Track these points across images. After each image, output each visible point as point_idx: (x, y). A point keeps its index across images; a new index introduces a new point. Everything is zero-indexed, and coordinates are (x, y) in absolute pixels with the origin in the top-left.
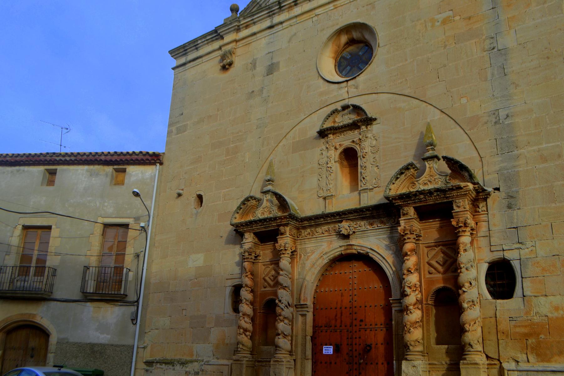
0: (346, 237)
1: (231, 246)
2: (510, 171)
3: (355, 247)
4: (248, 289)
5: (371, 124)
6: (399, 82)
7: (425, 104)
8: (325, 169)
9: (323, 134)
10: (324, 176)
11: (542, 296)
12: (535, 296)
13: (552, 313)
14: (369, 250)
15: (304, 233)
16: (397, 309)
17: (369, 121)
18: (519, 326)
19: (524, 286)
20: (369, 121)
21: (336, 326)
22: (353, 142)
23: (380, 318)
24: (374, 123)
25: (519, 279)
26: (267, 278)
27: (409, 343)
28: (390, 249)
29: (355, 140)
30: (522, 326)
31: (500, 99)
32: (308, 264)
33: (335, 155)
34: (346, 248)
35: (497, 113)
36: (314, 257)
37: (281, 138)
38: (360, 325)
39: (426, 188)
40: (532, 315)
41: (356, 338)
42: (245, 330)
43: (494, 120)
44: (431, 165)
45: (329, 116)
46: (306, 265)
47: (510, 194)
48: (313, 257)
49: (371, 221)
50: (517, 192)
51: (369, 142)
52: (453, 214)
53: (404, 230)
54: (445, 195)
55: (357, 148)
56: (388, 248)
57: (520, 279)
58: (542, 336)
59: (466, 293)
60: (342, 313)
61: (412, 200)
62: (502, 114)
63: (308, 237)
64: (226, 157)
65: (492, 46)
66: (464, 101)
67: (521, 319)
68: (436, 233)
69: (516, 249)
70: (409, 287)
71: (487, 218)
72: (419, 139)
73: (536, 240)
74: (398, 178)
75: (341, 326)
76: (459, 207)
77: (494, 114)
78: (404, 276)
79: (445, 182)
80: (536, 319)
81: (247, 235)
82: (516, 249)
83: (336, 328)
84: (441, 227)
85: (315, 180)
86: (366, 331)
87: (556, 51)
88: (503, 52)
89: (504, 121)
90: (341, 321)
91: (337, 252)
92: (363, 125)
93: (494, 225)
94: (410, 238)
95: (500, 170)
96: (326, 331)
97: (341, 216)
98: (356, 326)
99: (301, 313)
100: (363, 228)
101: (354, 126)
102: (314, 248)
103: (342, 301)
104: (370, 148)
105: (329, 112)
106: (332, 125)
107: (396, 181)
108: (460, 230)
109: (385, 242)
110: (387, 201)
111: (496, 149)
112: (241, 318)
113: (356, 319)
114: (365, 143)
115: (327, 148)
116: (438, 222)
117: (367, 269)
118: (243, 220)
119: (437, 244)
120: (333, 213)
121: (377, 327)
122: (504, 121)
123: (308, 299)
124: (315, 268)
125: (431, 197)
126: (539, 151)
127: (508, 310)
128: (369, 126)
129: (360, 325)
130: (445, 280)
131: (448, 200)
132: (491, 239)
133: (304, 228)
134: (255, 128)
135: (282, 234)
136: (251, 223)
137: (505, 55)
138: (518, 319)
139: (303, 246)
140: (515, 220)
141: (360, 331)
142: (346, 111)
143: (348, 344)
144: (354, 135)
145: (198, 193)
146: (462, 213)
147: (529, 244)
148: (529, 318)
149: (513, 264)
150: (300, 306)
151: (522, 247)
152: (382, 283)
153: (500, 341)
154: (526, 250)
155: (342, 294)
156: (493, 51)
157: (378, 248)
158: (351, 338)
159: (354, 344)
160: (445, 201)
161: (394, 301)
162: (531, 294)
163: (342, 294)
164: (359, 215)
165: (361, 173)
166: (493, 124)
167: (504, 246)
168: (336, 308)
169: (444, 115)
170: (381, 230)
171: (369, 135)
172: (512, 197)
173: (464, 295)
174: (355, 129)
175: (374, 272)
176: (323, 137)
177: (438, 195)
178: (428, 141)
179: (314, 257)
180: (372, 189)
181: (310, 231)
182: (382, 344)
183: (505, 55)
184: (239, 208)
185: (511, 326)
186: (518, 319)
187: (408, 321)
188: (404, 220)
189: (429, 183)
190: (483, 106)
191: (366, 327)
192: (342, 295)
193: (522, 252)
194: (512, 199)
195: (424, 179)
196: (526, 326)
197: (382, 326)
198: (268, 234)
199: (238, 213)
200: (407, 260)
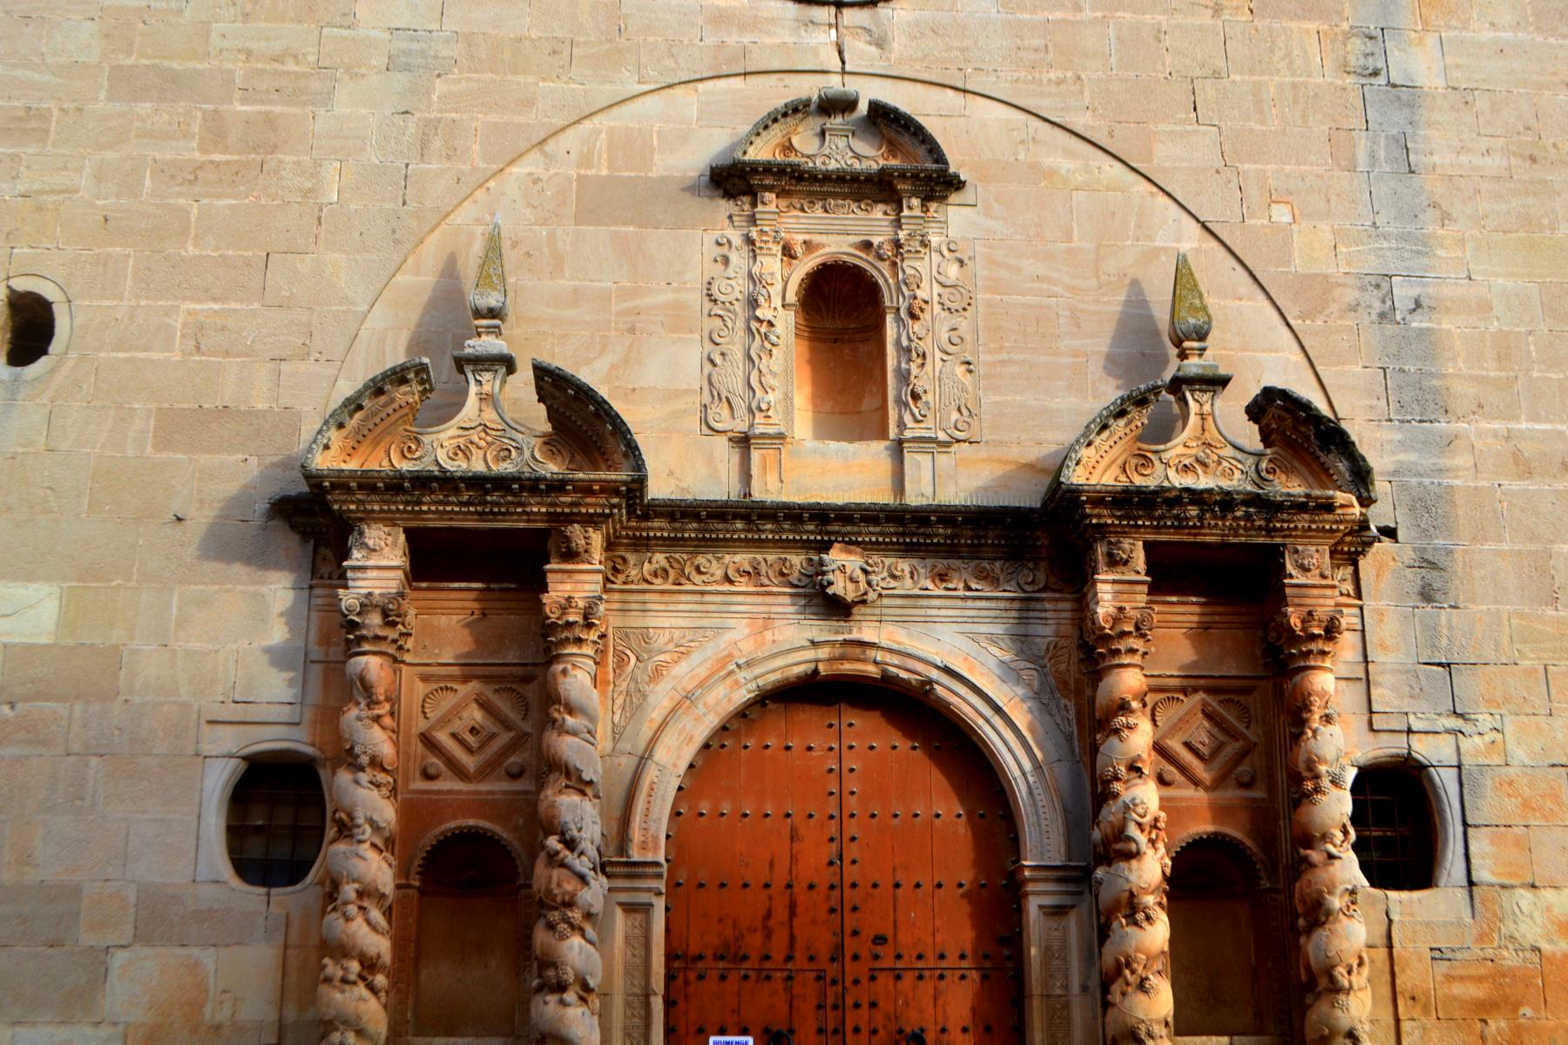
0: (838, 609)
1: (238, 569)
2: (1427, 481)
3: (880, 656)
4: (382, 777)
5: (942, 199)
6: (1053, 75)
7: (1144, 186)
8: (740, 324)
9: (733, 180)
10: (737, 354)
11: (1523, 886)
12: (1503, 887)
13: (1551, 941)
14: (934, 674)
15: (641, 566)
16: (1048, 901)
17: (940, 183)
18: (1461, 978)
19: (1476, 848)
20: (940, 183)
21: (767, 958)
22: (867, 246)
23: (955, 933)
24: (954, 198)
25: (1454, 829)
26: (443, 737)
27: (1143, 1028)
28: (1019, 680)
29: (876, 240)
30: (1471, 978)
31: (1394, 244)
32: (661, 698)
33: (784, 282)
34: (838, 651)
35: (1385, 285)
36: (684, 672)
37: (523, 146)
38: (876, 957)
39: (1188, 481)
40: (1496, 944)
41: (857, 1006)
42: (370, 965)
43: (1377, 306)
44: (1207, 408)
45: (775, 120)
46: (652, 699)
47: (1428, 556)
48: (682, 668)
49: (941, 564)
50: (1449, 552)
51: (943, 261)
52: (1288, 591)
53: (1116, 621)
54: (1268, 521)
55: (882, 274)
56: (1009, 673)
57: (1459, 829)
58: (1527, 1010)
59: (1337, 863)
60: (792, 907)
61: (1151, 518)
62: (1404, 293)
63: (659, 584)
64: (203, 149)
65: (1371, 63)
66: (1281, 214)
67: (1466, 955)
68: (1186, 643)
69: (1448, 732)
70: (1139, 825)
71: (1357, 620)
72: (1127, 302)
73: (1503, 711)
74: (1105, 427)
75: (789, 958)
76: (1305, 569)
77: (1378, 286)
78: (1117, 786)
79: (1254, 476)
80: (1510, 959)
81: (374, 534)
82: (1448, 732)
83: (767, 965)
84: (1204, 627)
85: (691, 356)
86: (898, 978)
87: (1555, 145)
88: (1404, 95)
89: (1408, 317)
90: (792, 938)
91: (795, 665)
92: (914, 194)
93: (1383, 647)
94: (1132, 651)
95: (1396, 472)
96: (723, 978)
97: (824, 524)
98: (855, 958)
99: (624, 897)
100: (906, 586)
101: (876, 188)
102: (690, 635)
103: (794, 859)
104: (937, 289)
105: (779, 103)
106: (779, 158)
107: (1099, 433)
108: (1313, 646)
109: (995, 650)
110: (306, 489)
111: (1383, 402)
112: (352, 909)
113: (855, 933)
114: (917, 264)
115: (750, 241)
116: (1196, 609)
117: (903, 744)
118: (352, 465)
119: (469, 670)
120: (802, 507)
121: (944, 964)
122: (1408, 317)
123: (651, 834)
124: (698, 719)
125: (1223, 518)
126: (1508, 438)
127: (1428, 924)
128: (933, 206)
129: (876, 957)
130: (1220, 812)
131: (1268, 541)
132: (1375, 692)
133: (642, 544)
134: (379, 61)
135: (571, 555)
136: (396, 485)
137: (1411, 106)
138: (1458, 955)
139: (635, 621)
140: (1444, 642)
141: (873, 978)
142: (837, 121)
143: (820, 1031)
144: (874, 222)
145: (22, 285)
146: (1315, 592)
147: (1485, 721)
148: (1490, 953)
149: (1437, 779)
150: (618, 864)
151: (1467, 728)
152: (962, 799)
153: (1406, 1026)
154: (1477, 739)
155: (793, 830)
156: (1373, 80)
157: (971, 669)
158: (835, 1007)
159: (849, 1027)
160: (1261, 540)
161: (1037, 874)
162: (1493, 880)
163: (793, 830)
164: (903, 534)
165: (904, 377)
166: (1374, 317)
167: (1412, 717)
168: (767, 886)
169: (1214, 244)
170: (983, 604)
171: (934, 240)
172: (1433, 565)
173: (1331, 869)
174: (876, 202)
175: (931, 757)
176: (729, 195)
177: (1248, 517)
178: (1192, 321)
179: (684, 672)
180: (947, 444)
181: (664, 563)
182: (965, 1030)
183: (1411, 106)
184: (353, 405)
185: (1439, 978)
186: (1458, 955)
187: (1138, 950)
188: (1114, 582)
189: (1199, 469)
190: (1342, 249)
191: (899, 965)
192: (793, 837)
193: (1465, 744)
194: (1435, 573)
195: (1180, 450)
196: (1480, 979)
197: (965, 964)
198: (492, 548)
199: (341, 426)
200: (1129, 728)
